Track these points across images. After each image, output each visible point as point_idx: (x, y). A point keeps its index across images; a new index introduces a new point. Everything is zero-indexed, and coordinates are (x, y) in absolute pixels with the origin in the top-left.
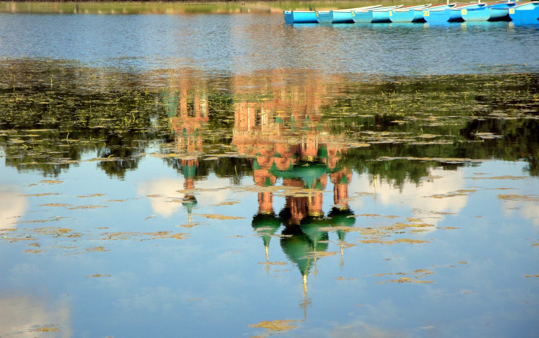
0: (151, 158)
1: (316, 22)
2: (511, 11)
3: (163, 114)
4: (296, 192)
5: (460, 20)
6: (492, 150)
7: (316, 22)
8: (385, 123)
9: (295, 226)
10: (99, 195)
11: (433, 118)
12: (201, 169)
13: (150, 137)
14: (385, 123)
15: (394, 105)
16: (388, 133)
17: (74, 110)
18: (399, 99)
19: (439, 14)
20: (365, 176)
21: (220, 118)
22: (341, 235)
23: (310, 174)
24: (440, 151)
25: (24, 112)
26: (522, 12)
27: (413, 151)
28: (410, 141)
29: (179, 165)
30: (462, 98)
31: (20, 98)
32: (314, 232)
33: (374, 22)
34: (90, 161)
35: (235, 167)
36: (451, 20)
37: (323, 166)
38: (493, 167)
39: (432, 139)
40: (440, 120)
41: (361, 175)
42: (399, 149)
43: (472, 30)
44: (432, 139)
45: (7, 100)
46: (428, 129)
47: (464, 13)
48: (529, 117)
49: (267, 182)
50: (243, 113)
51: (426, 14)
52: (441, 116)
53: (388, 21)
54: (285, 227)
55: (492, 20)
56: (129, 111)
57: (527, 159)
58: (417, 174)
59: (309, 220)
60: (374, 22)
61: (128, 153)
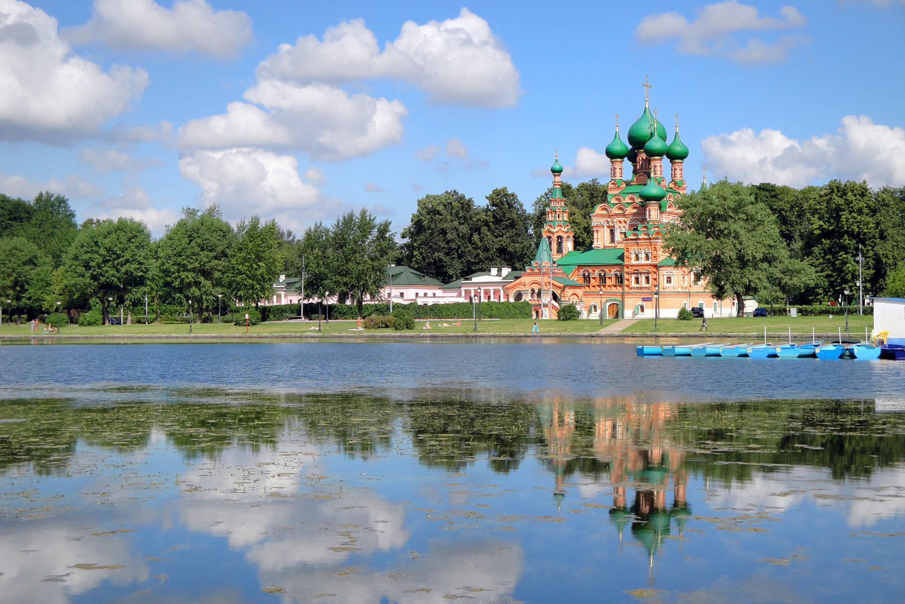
0: (530, 458)
1: (661, 355)
2: (817, 351)
3: (539, 425)
4: (645, 487)
5: (776, 356)
6: (801, 458)
7: (661, 355)
8: (718, 435)
9: (644, 515)
10: (113, 533)
11: (759, 432)
12: (569, 469)
13: (527, 441)
14: (718, 435)
15: (728, 420)
16: (722, 443)
17: (472, 419)
18: (730, 416)
19: (759, 350)
20: (700, 477)
21: (585, 427)
22: (679, 522)
23: (656, 475)
24: (759, 458)
25: (437, 421)
26: (825, 351)
27: (739, 457)
28: (741, 448)
29: (551, 465)
30: (780, 416)
31: (434, 410)
32: (660, 521)
33: (707, 356)
34: (482, 462)
35: (595, 467)
36: (770, 356)
37: (666, 470)
38: (800, 471)
39: (759, 449)
40: (764, 434)
41: (192, 462)
42: (728, 455)
43: (786, 362)
44: (759, 449)
45: (425, 412)
46: (757, 441)
47: (778, 351)
48: (835, 433)
49: (620, 479)
50: (603, 427)
51: (749, 351)
52: (766, 431)
53: (719, 355)
54: (398, 107)
55: (800, 357)
56: (516, 421)
57: (830, 467)
58: (743, 475)
59: (654, 510)
60: (707, 356)
61: (512, 454)
